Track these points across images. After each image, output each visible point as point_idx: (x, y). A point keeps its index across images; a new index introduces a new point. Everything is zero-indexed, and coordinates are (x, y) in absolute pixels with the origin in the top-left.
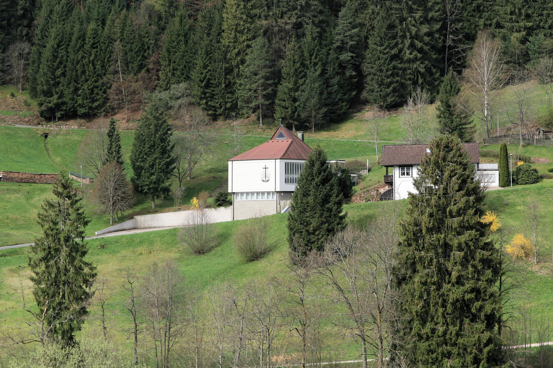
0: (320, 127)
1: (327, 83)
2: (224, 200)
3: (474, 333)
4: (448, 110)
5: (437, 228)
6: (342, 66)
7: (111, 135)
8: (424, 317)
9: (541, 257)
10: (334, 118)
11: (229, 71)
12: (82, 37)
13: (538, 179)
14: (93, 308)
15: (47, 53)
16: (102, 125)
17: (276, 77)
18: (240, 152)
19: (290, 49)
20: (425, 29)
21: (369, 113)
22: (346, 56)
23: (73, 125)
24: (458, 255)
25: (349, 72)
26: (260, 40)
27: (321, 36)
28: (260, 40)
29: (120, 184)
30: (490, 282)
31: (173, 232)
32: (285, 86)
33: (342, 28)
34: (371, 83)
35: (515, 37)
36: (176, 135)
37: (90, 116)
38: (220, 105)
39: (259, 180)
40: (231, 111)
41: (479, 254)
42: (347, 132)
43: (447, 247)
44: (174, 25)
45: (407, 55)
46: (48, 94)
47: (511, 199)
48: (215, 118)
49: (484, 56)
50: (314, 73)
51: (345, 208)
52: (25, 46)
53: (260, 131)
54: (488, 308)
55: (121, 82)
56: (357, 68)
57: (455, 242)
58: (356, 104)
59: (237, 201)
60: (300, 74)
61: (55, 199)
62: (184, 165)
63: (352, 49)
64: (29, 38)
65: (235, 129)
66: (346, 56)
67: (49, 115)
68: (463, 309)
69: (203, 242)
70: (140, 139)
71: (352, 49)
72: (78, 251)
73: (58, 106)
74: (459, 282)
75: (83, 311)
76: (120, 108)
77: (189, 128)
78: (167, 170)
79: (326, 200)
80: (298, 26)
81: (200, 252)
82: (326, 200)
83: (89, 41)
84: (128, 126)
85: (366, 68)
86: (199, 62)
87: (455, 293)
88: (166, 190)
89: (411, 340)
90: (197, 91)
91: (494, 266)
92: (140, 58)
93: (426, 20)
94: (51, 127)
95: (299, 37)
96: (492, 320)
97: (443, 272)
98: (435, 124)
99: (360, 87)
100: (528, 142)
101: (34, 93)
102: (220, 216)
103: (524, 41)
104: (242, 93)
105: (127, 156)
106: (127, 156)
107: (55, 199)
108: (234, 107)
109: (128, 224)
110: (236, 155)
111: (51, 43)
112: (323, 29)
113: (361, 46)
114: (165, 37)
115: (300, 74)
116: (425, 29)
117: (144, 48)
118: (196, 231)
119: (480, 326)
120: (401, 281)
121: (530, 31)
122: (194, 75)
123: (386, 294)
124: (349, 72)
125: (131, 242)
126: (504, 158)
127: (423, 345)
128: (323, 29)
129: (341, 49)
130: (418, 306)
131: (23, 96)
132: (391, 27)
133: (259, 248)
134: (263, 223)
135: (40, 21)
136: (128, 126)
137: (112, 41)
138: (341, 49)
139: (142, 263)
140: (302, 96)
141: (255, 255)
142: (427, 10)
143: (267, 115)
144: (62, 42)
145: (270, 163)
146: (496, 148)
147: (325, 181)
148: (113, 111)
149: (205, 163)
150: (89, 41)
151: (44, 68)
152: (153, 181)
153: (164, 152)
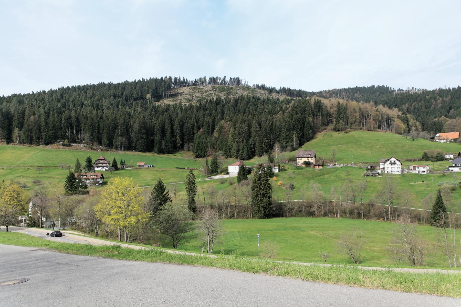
0: (247, 160)
1: (248, 151)
2: (228, 173)
3: (266, 199)
4: (270, 157)
5: (259, 180)
6: (251, 148)
7: (207, 161)
8: (257, 196)
9: (284, 185)
10: (250, 158)
11: (230, 149)
12: (202, 142)
13: (285, 171)
14: (197, 194)
15: (196, 145)
16: (205, 159)
17: (238, 150)
18: (231, 164)
19: (241, 144)
20: (267, 141)
21: (256, 157)
22: (252, 146)
23: (201, 159)
24: (263, 185)
25: (253, 149)
26: (236, 143)
27: (247, 142)
28: (236, 143)
29: (208, 170)
30: (269, 190)
31: (217, 179)
32: (240, 152)
33: (251, 141)
34: (257, 151)
35: (284, 143)
36: (219, 161)
37: (204, 157)
38: (228, 155)
39: (234, 170)
40: (231, 157)
41: (267, 185)
42: (252, 161)
43: (261, 184)
44: (220, 140)
45: (264, 146)
46: (196, 153)
47: (280, 174)
48: (227, 158)
49: (277, 146)
50: (246, 149)
51: (248, 176)
52: (192, 144)
53: (236, 160)
54: (268, 195)
55: (210, 151)
56: (254, 148)
57: (262, 183)
58: (254, 155)
59: (230, 173)
60: (243, 149)
61: (189, 174)
62: (221, 167)
63: (253, 145)
64: (193, 142)
65: (229, 160)
66: (252, 146)
67: (197, 157)
68: (264, 195)
69: (223, 182)
70: (212, 162)
71: (253, 145)
72: (194, 183)
73: (198, 155)
74: (263, 190)
75: (195, 194)
76: (210, 155)
77: (221, 159)
78: (217, 167)
79: (244, 174)
80: (243, 140)
81: (222, 183)
82: (244, 174)
83: (204, 143)
84: (210, 159)
85: (256, 148)
86: (224, 147)
87: (262, 192)
88: (217, 171)
89: (254, 201)
90: (224, 153)
91: (270, 188)
92: (213, 146)
93: (267, 139)
94: (197, 159)
95: (243, 142)
96: (269, 197)
97: (260, 189)
98: (267, 160)
99: (255, 152)
100: (284, 163)
101: (194, 153)
102: (227, 176)
103: (286, 144)
104: (232, 153)
105: (210, 164)
106: (210, 164)
107: (189, 174)
108: (231, 156)
109: (210, 178)
110: (230, 165)
111: (197, 143)
112: (247, 141)
113: (255, 144)
114: (218, 142)
115: (243, 149)
116: (267, 141)
117: (214, 144)
118: (221, 179)
119: (267, 198)
120: (253, 190)
121: (287, 142)
122: (223, 149)
123: (251, 193)
124: (253, 149)
125: (210, 181)
126: (279, 166)
127: (257, 202)
128: (247, 141)
129: (251, 145)
130: (256, 194)
131: (192, 153)
132: (260, 141)
133: (232, 183)
134: (233, 178)
135: (195, 139)
136: (210, 159)
137: (208, 143)
138: (251, 145)
139: (211, 184)
140: (243, 154)
141: (231, 184)
142: (267, 137)
143: (237, 157)
144: (199, 143)
145: (236, 167)
146: (278, 164)
147: (244, 171)
148: (208, 156)
149: (225, 166)
150: (204, 143)
151: (195, 148)
152: (215, 169)
153: (216, 164)
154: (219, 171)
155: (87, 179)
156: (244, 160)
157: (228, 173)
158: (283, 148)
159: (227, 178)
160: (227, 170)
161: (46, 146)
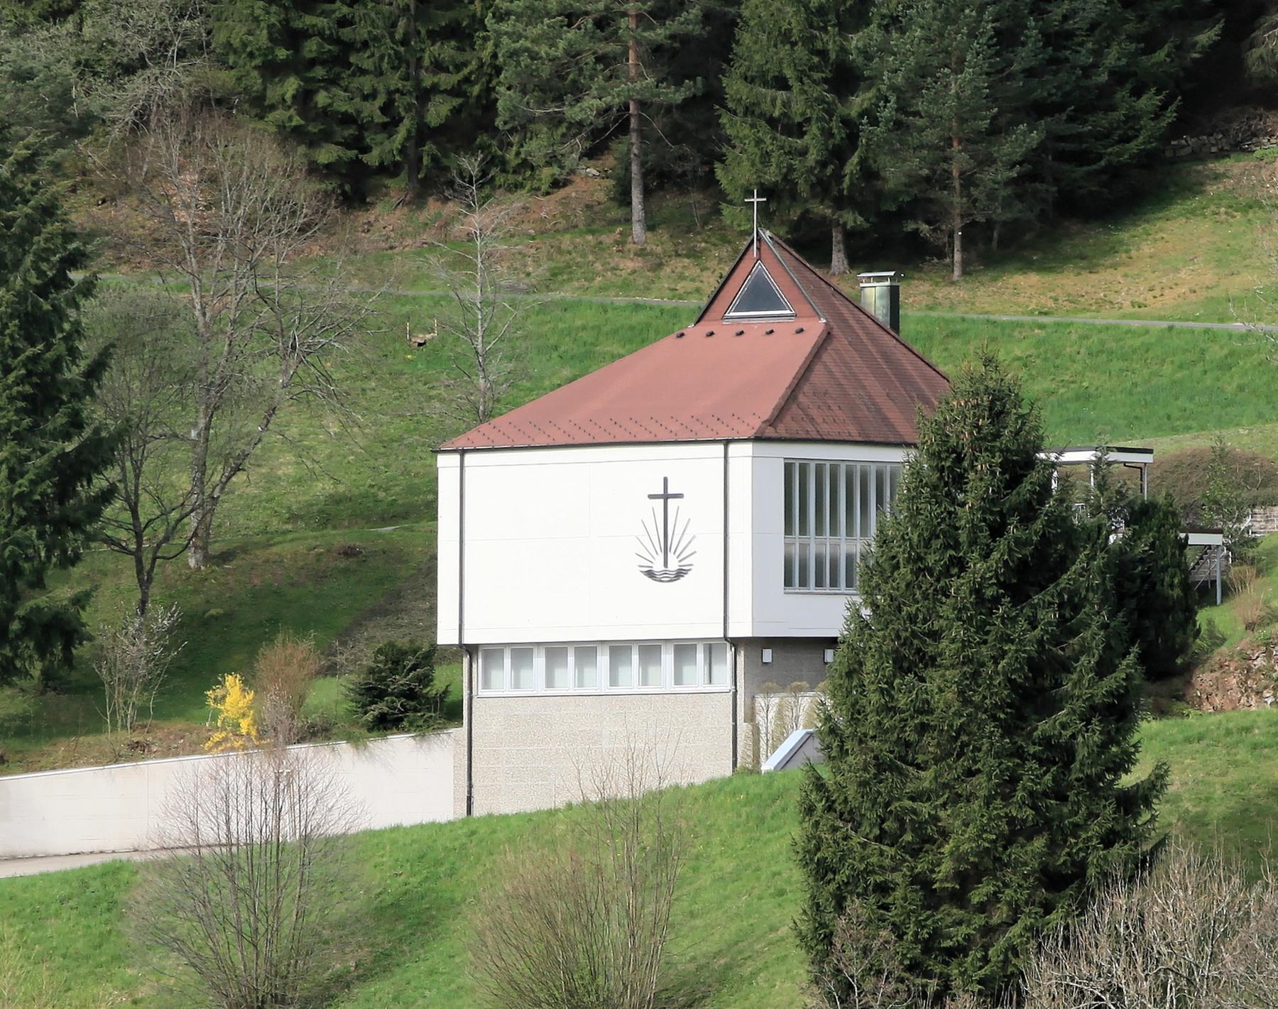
2: (411, 693)
18: (523, 388)
31: (100, 890)
36: (117, 292)
40: (456, 148)
48: (354, 187)
53: (632, 268)
59: (492, 695)
62: (166, 477)
65: (477, 257)
79: (1034, 691)
82: (1034, 691)
88: (60, 631)
102: (389, 787)
108: (475, 122)
110: (486, 417)
134: (649, 833)
143: (675, 171)
145: (694, 467)
147: (1025, 578)
149: (294, 463)
154: (122, 624)
155: (293, 444)
156: (894, 238)
157: (411, 693)
158: (1024, 821)
159: (429, 850)
160: (407, 578)
161: (363, 217)
